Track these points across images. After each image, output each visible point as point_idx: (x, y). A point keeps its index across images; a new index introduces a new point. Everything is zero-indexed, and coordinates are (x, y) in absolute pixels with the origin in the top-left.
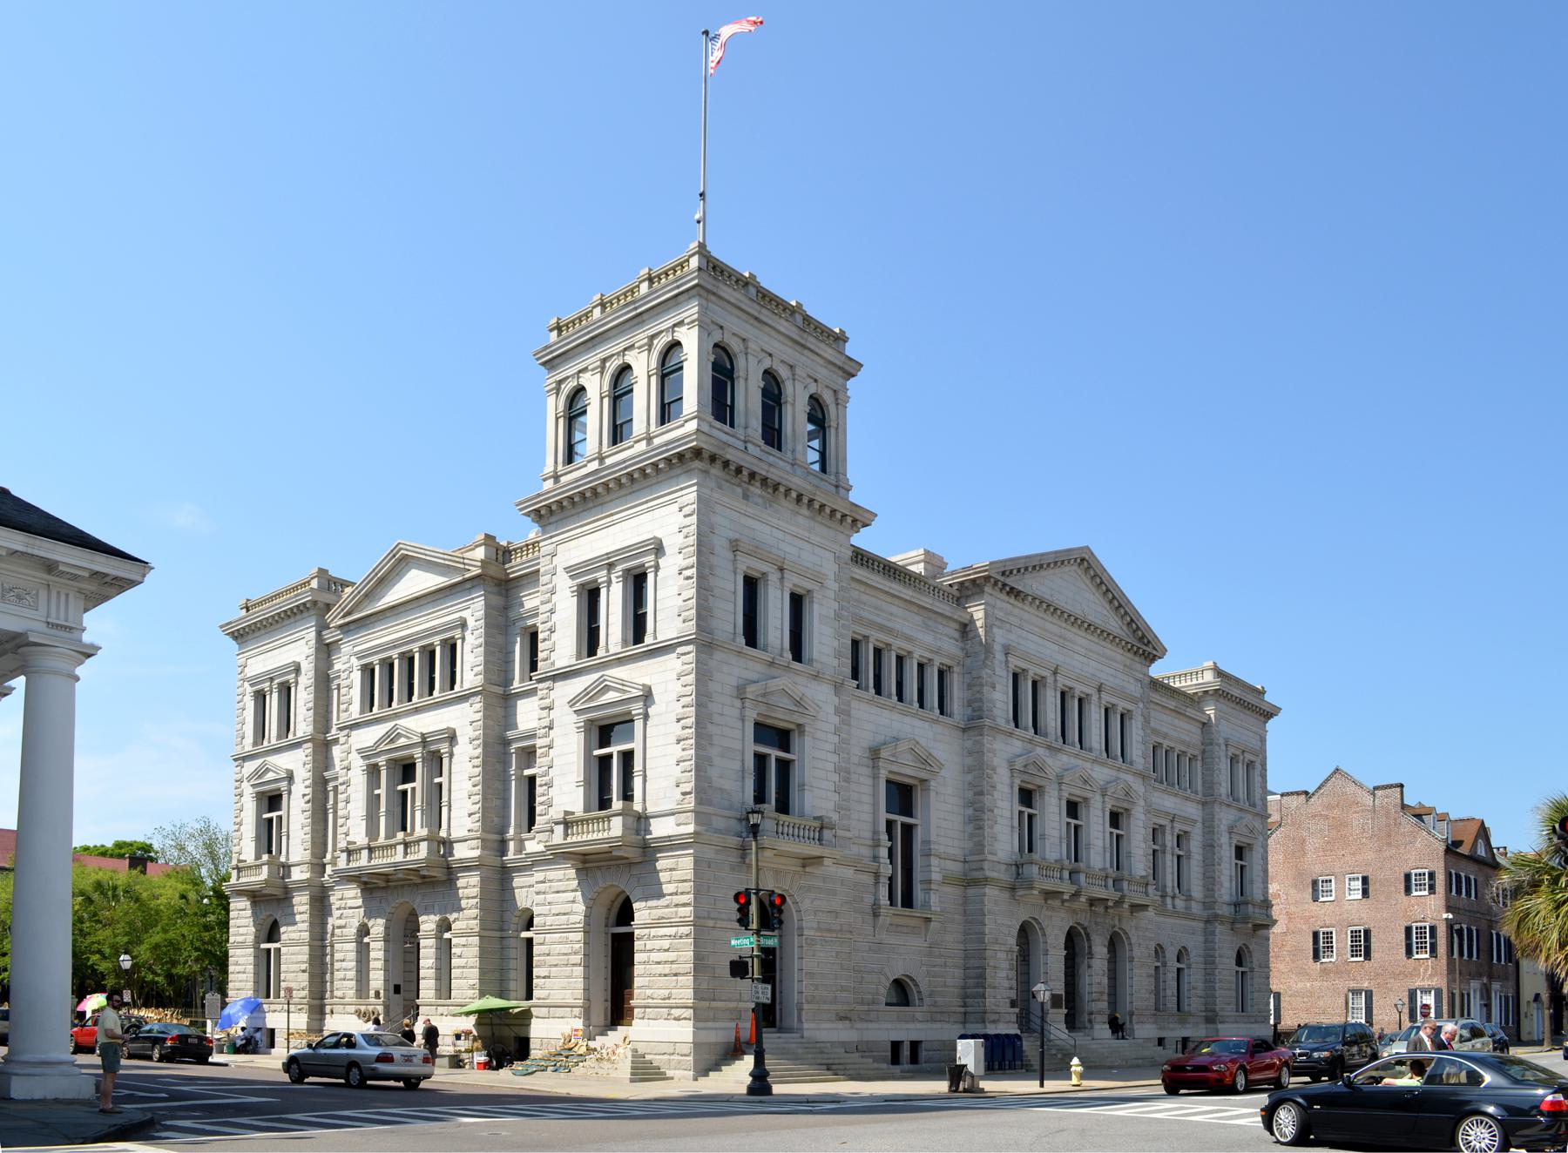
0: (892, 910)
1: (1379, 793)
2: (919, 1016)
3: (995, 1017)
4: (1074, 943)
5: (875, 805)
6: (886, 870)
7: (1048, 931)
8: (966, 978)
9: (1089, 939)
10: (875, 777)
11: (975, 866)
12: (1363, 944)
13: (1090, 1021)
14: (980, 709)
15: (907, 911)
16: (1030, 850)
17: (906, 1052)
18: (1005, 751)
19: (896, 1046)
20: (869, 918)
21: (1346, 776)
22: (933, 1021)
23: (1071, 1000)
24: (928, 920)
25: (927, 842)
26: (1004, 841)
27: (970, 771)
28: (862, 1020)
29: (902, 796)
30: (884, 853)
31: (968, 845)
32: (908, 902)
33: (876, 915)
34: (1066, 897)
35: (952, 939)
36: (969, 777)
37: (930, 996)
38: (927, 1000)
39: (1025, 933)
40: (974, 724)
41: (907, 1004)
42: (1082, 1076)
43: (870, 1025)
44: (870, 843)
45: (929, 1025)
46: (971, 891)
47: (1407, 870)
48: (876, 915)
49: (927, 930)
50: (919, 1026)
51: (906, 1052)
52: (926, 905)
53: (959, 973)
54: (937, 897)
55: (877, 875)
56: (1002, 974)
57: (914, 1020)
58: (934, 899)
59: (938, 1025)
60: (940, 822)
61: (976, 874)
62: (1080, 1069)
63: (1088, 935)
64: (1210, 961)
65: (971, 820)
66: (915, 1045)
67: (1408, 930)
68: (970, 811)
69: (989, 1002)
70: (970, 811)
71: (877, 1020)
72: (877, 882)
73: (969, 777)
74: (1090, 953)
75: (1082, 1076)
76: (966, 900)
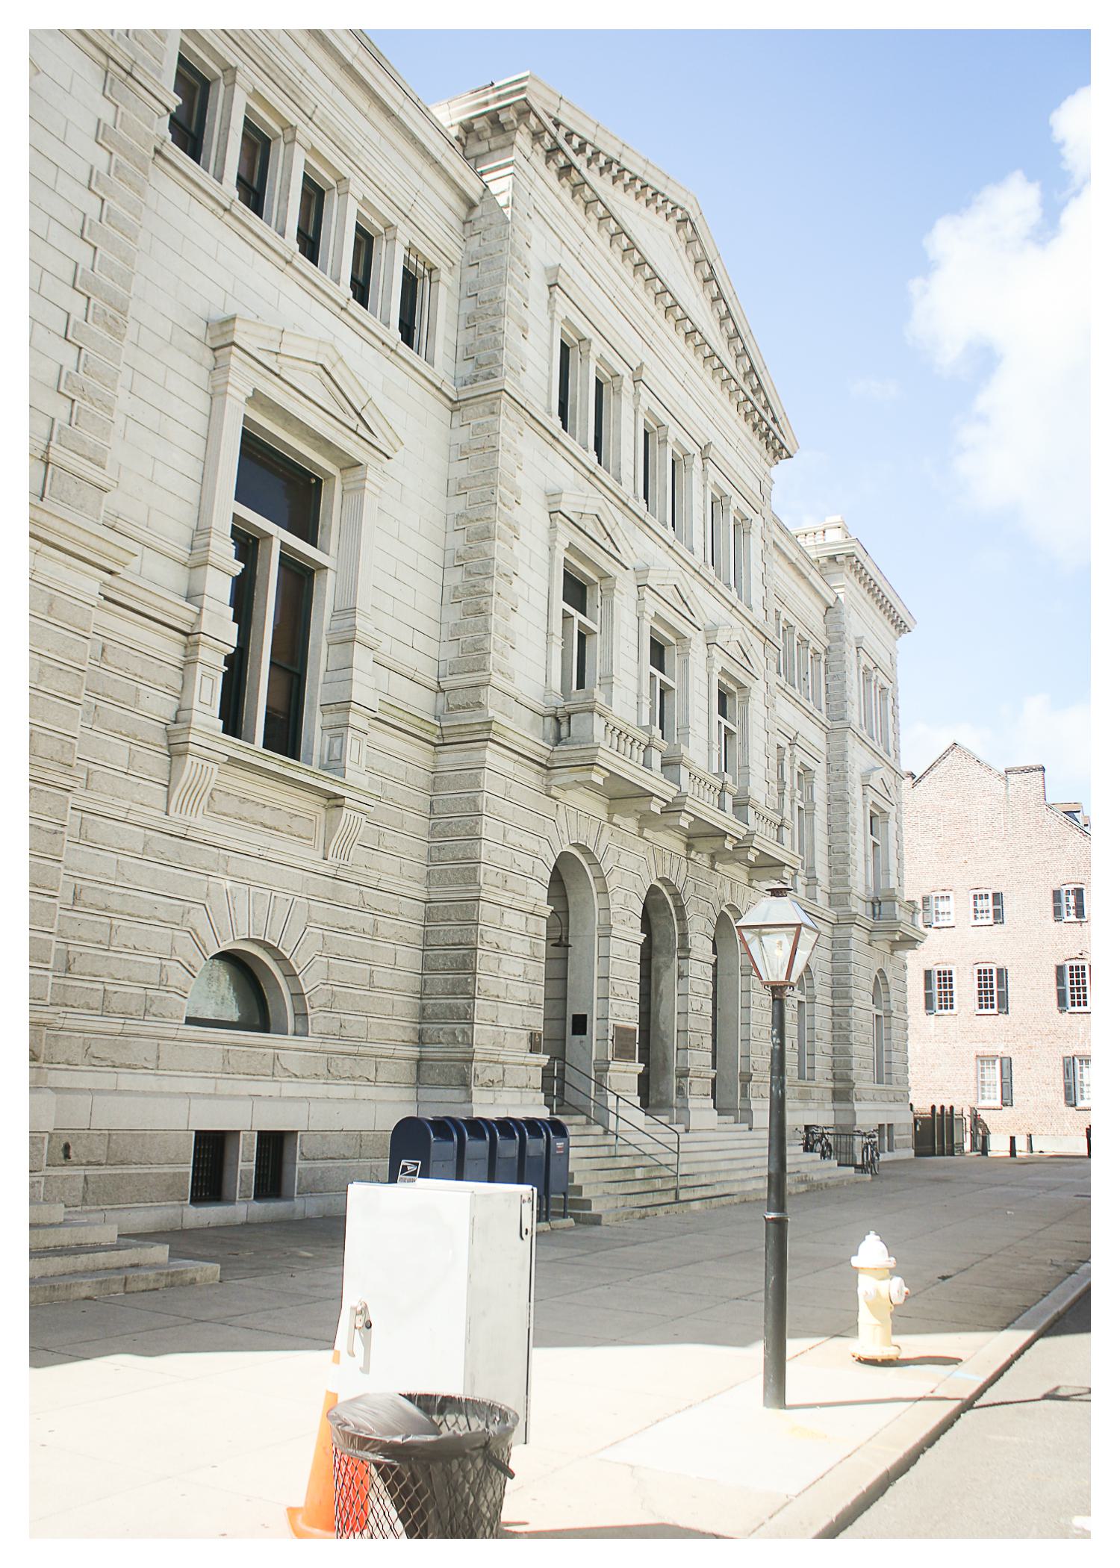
0: (231, 746)
1: (1012, 778)
2: (292, 1060)
3: (493, 1073)
4: (658, 913)
5: (205, 481)
6: (221, 629)
7: (612, 882)
8: (427, 967)
9: (682, 918)
10: (216, 395)
11: (460, 698)
12: (994, 989)
13: (680, 1090)
14: (494, 361)
15: (276, 762)
16: (581, 684)
17: (245, 1162)
18: (537, 468)
19: (212, 1148)
20: (155, 762)
21: (968, 755)
22: (331, 1075)
23: (647, 1041)
24: (334, 801)
25: (347, 611)
26: (526, 659)
27: (461, 490)
28: (95, 1061)
29: (282, 482)
30: (219, 587)
31: (451, 652)
32: (285, 735)
33: (175, 751)
34: (656, 807)
35: (395, 867)
36: (459, 505)
37: (329, 1008)
38: (318, 1021)
39: (563, 879)
40: (475, 392)
41: (265, 1027)
42: (904, 1320)
43: (126, 1080)
44: (183, 554)
45: (320, 1090)
46: (450, 758)
47: (1056, 887)
48: (175, 751)
49: (330, 830)
50: (290, 1089)
51: (245, 1162)
52: (334, 764)
53: (410, 958)
54: (371, 754)
55: (190, 637)
56: (514, 967)
57: (275, 1069)
58: (354, 750)
59: (344, 1090)
60: (381, 567)
61: (465, 717)
62: (895, 1288)
63: (681, 909)
64: (840, 991)
65: (460, 561)
66: (274, 1146)
67: (1060, 970)
68: (456, 577)
69: (482, 1036)
70: (456, 577)
71: (156, 1066)
72: (189, 663)
73: (459, 505)
74: (685, 948)
75: (904, 1320)
76: (437, 779)
